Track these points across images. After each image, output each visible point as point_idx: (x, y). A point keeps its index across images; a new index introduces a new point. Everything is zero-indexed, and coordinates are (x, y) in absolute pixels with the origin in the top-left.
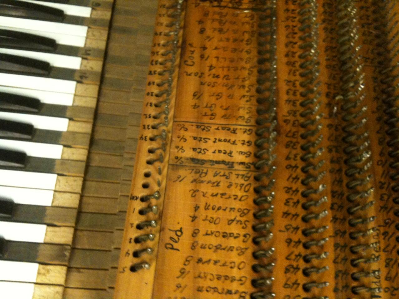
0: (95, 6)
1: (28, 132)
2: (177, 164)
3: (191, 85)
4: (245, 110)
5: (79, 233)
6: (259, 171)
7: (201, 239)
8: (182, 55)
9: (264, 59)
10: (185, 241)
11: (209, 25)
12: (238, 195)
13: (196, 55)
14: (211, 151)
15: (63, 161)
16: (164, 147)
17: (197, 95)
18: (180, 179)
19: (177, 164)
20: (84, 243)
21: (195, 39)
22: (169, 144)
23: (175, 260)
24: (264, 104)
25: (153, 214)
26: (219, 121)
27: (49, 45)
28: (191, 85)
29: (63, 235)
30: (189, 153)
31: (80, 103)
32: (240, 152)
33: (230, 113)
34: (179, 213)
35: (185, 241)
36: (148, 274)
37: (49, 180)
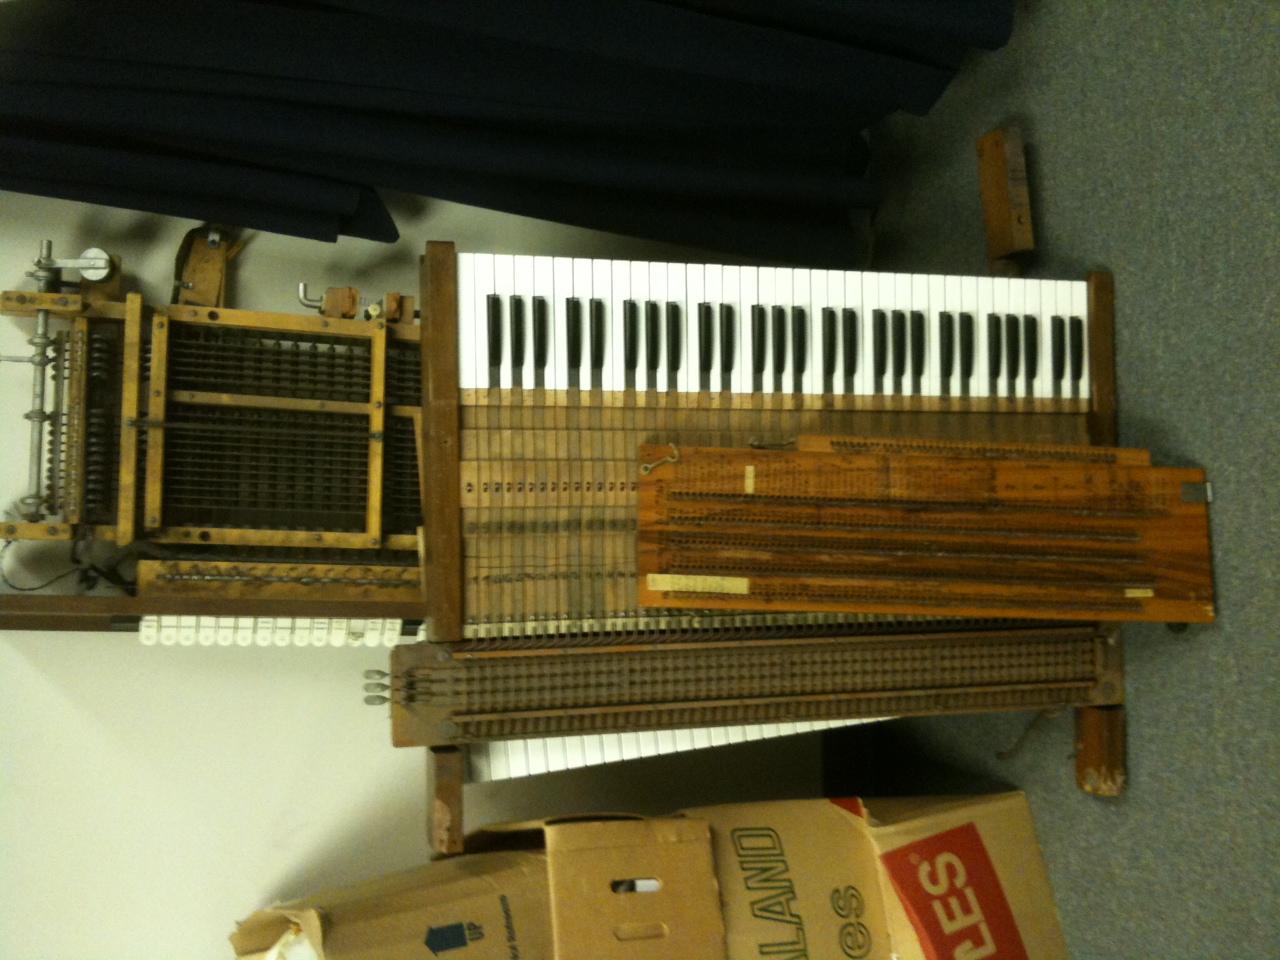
0: (1090, 401)
1: (1013, 374)
2: (885, 459)
3: (933, 464)
4: (922, 495)
5: (587, 410)
6: (886, 503)
7: (849, 473)
8: (951, 458)
9: (956, 506)
10: (845, 465)
11: (974, 473)
12: (872, 491)
13: (951, 466)
14: (895, 477)
15: (709, 394)
16: (894, 451)
17: (927, 468)
18: (877, 461)
19: (885, 459)
20: (952, 419)
21: (966, 465)
22: (927, 455)
23: (838, 462)
24: (926, 506)
25: (859, 450)
26: (913, 480)
27: (967, 372)
28: (933, 464)
29: (839, 405)
30: (893, 464)
31: (973, 403)
32: (896, 492)
33: (919, 487)
34: (860, 462)
35: (845, 465)
36: (829, 449)
37: (748, 388)
